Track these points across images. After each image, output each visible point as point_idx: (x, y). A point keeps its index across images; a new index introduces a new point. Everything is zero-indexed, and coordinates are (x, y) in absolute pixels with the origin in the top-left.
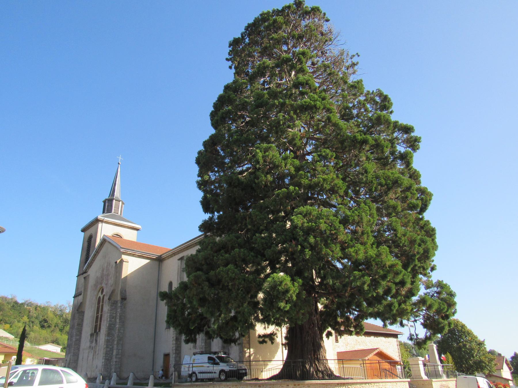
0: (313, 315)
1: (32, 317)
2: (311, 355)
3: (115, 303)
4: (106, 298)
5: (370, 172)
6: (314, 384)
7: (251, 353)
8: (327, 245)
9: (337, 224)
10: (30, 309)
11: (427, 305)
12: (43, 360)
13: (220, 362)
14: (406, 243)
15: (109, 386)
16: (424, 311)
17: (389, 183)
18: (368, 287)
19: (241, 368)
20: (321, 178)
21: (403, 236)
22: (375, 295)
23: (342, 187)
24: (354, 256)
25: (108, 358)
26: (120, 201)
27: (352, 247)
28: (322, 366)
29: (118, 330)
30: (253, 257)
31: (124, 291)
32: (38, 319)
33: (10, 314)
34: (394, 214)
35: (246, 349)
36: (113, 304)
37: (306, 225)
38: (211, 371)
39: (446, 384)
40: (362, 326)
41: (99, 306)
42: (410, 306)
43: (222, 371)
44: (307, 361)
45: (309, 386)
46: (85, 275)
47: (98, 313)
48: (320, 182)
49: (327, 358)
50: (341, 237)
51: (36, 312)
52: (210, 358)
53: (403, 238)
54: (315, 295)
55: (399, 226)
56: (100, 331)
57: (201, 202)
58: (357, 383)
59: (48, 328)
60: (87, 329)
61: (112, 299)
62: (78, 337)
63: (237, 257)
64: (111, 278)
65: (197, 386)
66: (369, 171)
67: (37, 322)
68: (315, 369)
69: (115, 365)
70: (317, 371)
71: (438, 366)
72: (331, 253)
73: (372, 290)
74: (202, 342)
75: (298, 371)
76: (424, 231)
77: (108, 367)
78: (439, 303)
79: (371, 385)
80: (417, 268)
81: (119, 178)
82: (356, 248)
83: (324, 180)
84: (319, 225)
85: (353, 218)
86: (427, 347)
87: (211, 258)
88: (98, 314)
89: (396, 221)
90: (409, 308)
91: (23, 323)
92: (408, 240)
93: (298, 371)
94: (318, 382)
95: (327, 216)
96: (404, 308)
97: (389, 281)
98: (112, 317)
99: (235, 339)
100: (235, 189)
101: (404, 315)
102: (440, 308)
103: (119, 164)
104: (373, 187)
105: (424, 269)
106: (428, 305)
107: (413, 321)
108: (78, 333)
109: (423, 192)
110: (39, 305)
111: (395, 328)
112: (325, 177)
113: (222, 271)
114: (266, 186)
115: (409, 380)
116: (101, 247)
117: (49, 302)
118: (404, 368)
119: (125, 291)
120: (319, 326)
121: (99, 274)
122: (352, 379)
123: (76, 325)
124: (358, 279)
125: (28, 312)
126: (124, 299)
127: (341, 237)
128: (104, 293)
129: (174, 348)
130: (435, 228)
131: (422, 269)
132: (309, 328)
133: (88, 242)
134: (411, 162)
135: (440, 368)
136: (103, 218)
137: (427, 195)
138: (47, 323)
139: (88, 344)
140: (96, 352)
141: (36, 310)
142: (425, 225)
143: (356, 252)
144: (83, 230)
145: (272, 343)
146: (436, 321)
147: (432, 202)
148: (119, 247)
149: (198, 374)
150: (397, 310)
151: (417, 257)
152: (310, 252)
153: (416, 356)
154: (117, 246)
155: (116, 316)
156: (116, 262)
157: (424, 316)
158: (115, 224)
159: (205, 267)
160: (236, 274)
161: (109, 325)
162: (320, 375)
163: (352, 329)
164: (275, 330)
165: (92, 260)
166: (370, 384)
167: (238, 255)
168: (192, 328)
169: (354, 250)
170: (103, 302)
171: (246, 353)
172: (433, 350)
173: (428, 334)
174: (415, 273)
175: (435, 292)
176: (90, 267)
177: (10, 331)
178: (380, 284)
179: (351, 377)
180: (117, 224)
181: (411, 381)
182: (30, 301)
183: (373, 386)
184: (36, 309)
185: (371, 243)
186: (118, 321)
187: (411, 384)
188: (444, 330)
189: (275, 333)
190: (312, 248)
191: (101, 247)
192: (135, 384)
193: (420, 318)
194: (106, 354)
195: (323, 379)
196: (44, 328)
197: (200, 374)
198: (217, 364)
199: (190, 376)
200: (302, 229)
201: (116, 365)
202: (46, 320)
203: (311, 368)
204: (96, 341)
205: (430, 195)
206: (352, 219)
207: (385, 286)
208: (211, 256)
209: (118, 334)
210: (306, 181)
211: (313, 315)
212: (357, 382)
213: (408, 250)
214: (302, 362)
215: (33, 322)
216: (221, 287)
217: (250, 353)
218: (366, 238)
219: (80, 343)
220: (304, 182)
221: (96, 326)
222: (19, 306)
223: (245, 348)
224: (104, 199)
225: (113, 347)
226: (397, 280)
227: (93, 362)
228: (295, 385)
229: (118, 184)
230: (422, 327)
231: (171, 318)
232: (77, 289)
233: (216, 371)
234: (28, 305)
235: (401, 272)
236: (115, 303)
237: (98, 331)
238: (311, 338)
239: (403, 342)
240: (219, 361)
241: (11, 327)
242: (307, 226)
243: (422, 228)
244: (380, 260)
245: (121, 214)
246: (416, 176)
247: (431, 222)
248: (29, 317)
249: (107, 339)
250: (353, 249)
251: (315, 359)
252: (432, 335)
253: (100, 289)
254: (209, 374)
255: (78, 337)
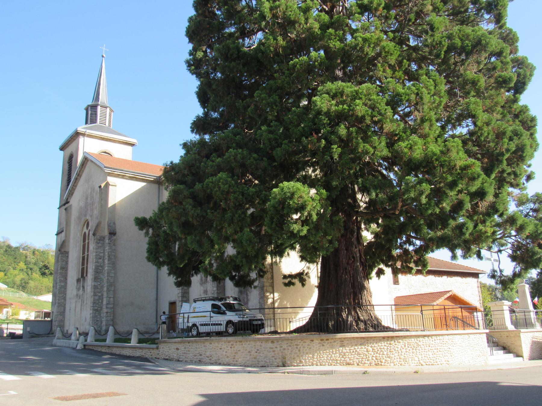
0: (354, 246)
1: (30, 263)
2: (349, 299)
3: (102, 239)
4: (91, 233)
5: (438, 29)
6: (350, 338)
7: (275, 299)
8: (366, 139)
9: (382, 106)
10: (26, 253)
11: (516, 226)
12: (42, 312)
13: (227, 310)
14: (490, 137)
15: (85, 343)
16: (513, 238)
17: (467, 44)
18: (427, 199)
19: (255, 318)
20: (361, 37)
21: (485, 125)
22: (437, 211)
23: (394, 52)
24: (406, 153)
25: (96, 308)
26: (106, 108)
27: (403, 141)
28: (364, 314)
29: (108, 273)
30: (255, 159)
31: (112, 224)
32: (37, 266)
33: (3, 260)
34: (473, 93)
35: (268, 294)
36: (99, 240)
37: (334, 108)
38: (207, 323)
39: (540, 336)
40: (425, 260)
41: (85, 244)
42: (491, 227)
43: (229, 322)
44: (343, 308)
45: (343, 341)
46: (67, 205)
47: (84, 253)
48: (358, 44)
49: (373, 303)
50: (388, 127)
51: (33, 257)
52: (214, 306)
53: (485, 129)
54: (357, 218)
55: (480, 110)
56: (87, 275)
57: (197, 94)
58: (411, 337)
59: (50, 276)
60: (73, 273)
61: (98, 235)
62: (63, 284)
63: (233, 161)
64: (96, 208)
65: (189, 343)
66: (436, 27)
67: (36, 268)
68: (355, 319)
69: (106, 317)
70: (358, 320)
71: (530, 312)
72: (372, 150)
73: (433, 204)
74: (214, 285)
75: (331, 322)
76: (519, 121)
77: (98, 319)
78: (536, 225)
79: (432, 339)
80: (505, 175)
81: (104, 77)
82: (410, 141)
83: (365, 40)
84: (354, 108)
85: (407, 97)
86: (514, 287)
87: (198, 164)
88: (85, 254)
89: (476, 103)
90: (490, 231)
91: (20, 270)
92: (494, 132)
93: (331, 322)
94: (355, 336)
95: (368, 95)
96: (481, 230)
97: (460, 192)
98: (99, 257)
99: (250, 280)
100: (233, 63)
101: (482, 242)
102: (537, 231)
103: (103, 56)
104: (441, 52)
105: (516, 175)
106: (518, 225)
107: (497, 252)
108: (62, 279)
109: (520, 63)
110: (37, 249)
111: (472, 263)
112: (368, 35)
113: (212, 182)
114: (277, 54)
115: (487, 331)
116: (82, 167)
117: (49, 245)
118: (486, 315)
119: (114, 224)
120: (362, 260)
121: (82, 204)
122: (407, 330)
123: (59, 268)
124: (412, 187)
125: (25, 258)
126: (113, 233)
127: (388, 127)
128: (89, 228)
129: (180, 295)
130: (535, 117)
131: (513, 177)
132: (348, 264)
133: (69, 163)
134: (503, 14)
135: (533, 315)
136: (84, 130)
137: (527, 67)
138: (48, 270)
139: (75, 292)
140: (84, 301)
141: (34, 255)
142: (520, 112)
143: (411, 148)
144: (62, 148)
145: (303, 285)
146: (530, 250)
147: (533, 79)
148: (102, 167)
149: (200, 327)
150: (471, 234)
151: (507, 156)
152: (340, 149)
153: (501, 300)
154: (100, 165)
155: (104, 257)
156: (100, 187)
157: (513, 245)
158: (101, 138)
159: (189, 178)
160: (230, 186)
161: (95, 267)
162: (362, 326)
163: (412, 265)
164: (305, 269)
165: (73, 186)
166: (430, 337)
167: (234, 159)
168: (181, 266)
169: (408, 145)
170: (88, 239)
171: (268, 298)
172: (524, 292)
173: (518, 269)
174: (501, 182)
175: (531, 209)
176: (72, 195)
177: (5, 280)
178: (447, 196)
179: (406, 328)
180: (104, 138)
181: (490, 332)
182: (26, 244)
183: (435, 340)
184: (34, 253)
185: (436, 135)
186: (106, 261)
187: (491, 336)
188: (540, 264)
189: (306, 272)
190: (345, 143)
191: (82, 167)
192: (116, 340)
193: (506, 248)
194: (94, 303)
195: (366, 330)
196: (45, 276)
197: (202, 327)
198: (224, 313)
199: (189, 329)
200: (328, 114)
201: (108, 316)
202: (47, 266)
203: (349, 317)
204: (83, 287)
205: (532, 68)
206: (406, 99)
207: (454, 198)
208: (197, 162)
209: (108, 279)
210: (336, 44)
211: (354, 246)
212: (411, 334)
213: (493, 146)
214: (337, 309)
215: (31, 269)
216: (212, 205)
217: (273, 299)
218: (427, 128)
219: (66, 291)
220: (334, 45)
221: (83, 269)
222: (13, 251)
223: (267, 291)
224: (85, 106)
225: (102, 295)
226: (473, 189)
227: (81, 313)
228: (322, 340)
229: (103, 84)
230: (509, 260)
231: (152, 253)
232: (60, 224)
233: (222, 323)
234: (24, 249)
235: (479, 176)
236: (102, 239)
237: (85, 275)
238: (350, 277)
239: (488, 285)
240: (224, 309)
241: (5, 275)
242: (336, 111)
243: (516, 116)
244: (447, 159)
245: (110, 125)
246: (511, 39)
247: (530, 107)
248: (26, 263)
249: (94, 285)
250: (407, 143)
251: (355, 304)
252: (523, 271)
253: (85, 223)
254: (217, 326)
255: (63, 284)
